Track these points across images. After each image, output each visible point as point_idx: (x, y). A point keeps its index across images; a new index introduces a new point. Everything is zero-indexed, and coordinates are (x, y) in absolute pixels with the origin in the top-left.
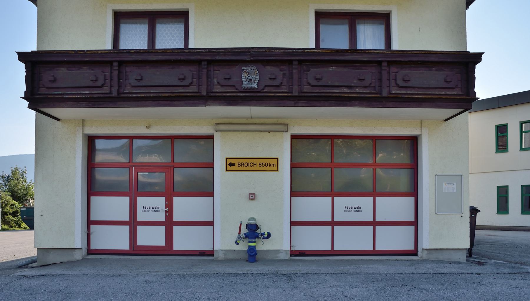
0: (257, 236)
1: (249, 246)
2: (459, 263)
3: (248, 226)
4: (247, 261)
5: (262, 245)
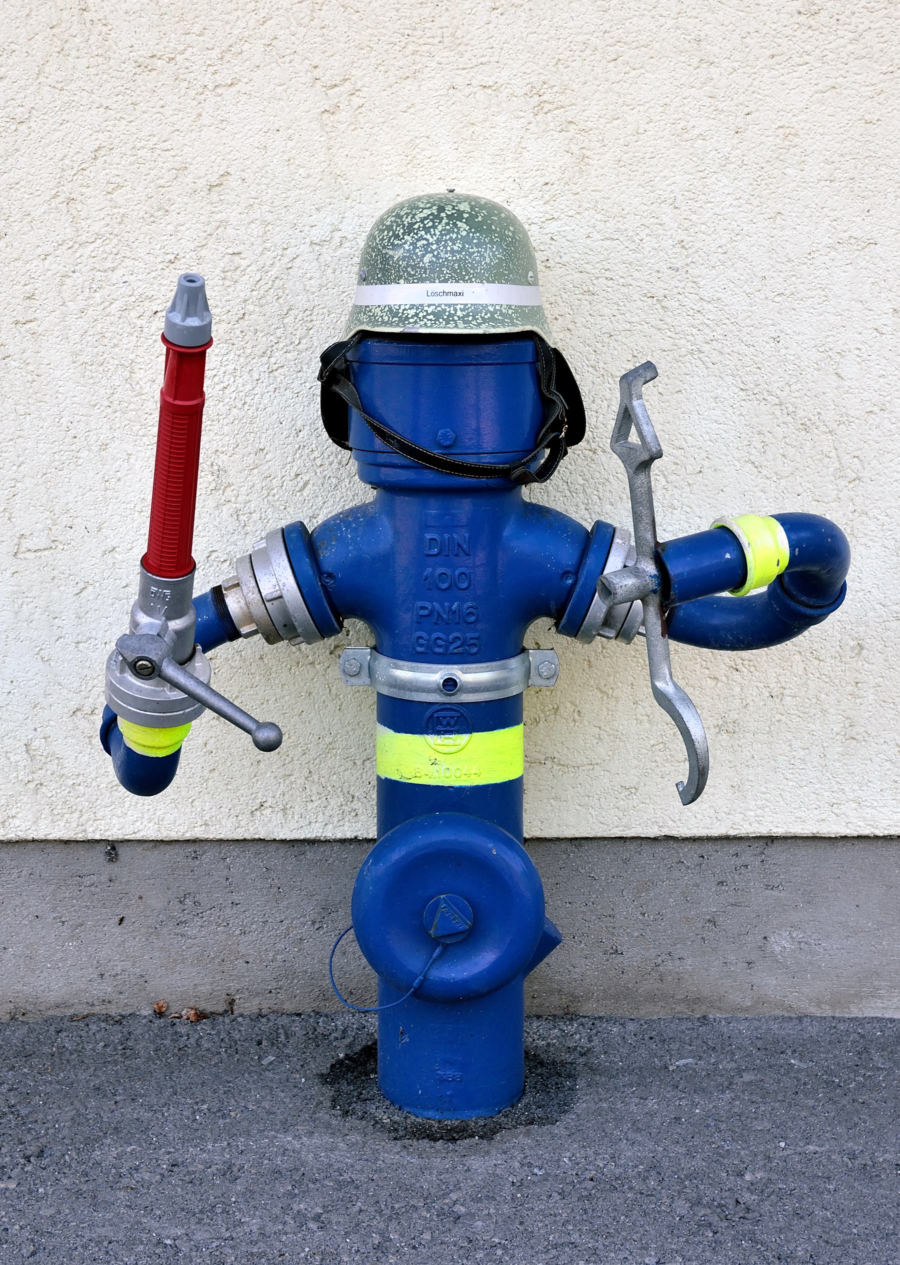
0: (558, 590)
1: (401, 801)
2: (655, 537)
3: (354, 383)
4: (354, 1072)
5: (609, 751)
